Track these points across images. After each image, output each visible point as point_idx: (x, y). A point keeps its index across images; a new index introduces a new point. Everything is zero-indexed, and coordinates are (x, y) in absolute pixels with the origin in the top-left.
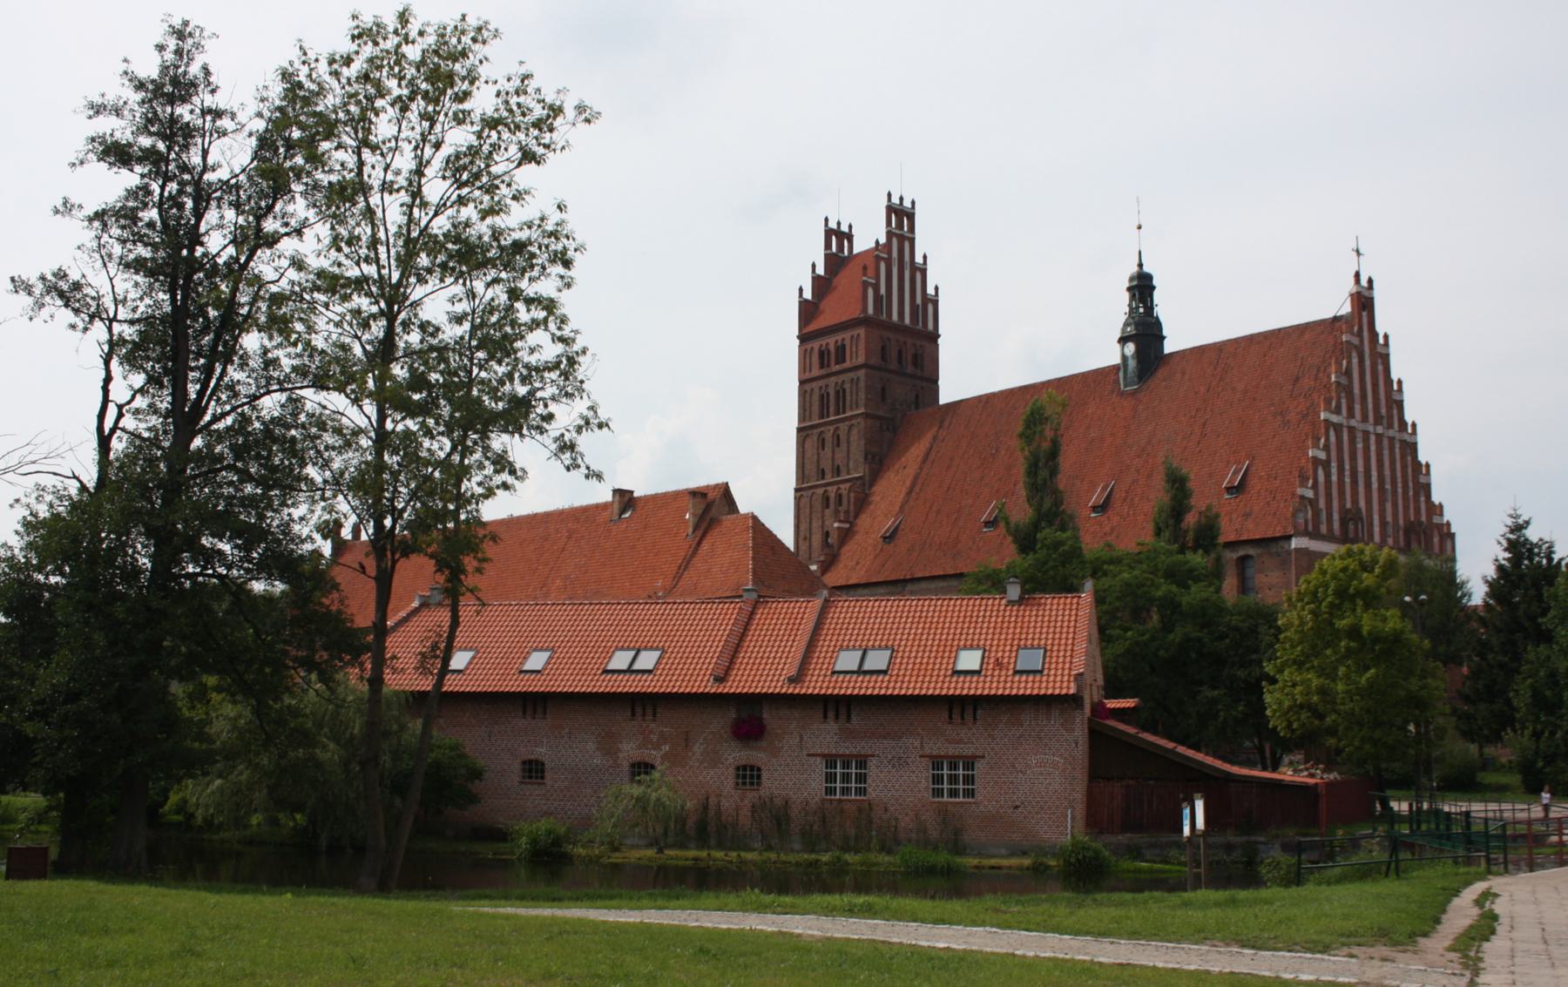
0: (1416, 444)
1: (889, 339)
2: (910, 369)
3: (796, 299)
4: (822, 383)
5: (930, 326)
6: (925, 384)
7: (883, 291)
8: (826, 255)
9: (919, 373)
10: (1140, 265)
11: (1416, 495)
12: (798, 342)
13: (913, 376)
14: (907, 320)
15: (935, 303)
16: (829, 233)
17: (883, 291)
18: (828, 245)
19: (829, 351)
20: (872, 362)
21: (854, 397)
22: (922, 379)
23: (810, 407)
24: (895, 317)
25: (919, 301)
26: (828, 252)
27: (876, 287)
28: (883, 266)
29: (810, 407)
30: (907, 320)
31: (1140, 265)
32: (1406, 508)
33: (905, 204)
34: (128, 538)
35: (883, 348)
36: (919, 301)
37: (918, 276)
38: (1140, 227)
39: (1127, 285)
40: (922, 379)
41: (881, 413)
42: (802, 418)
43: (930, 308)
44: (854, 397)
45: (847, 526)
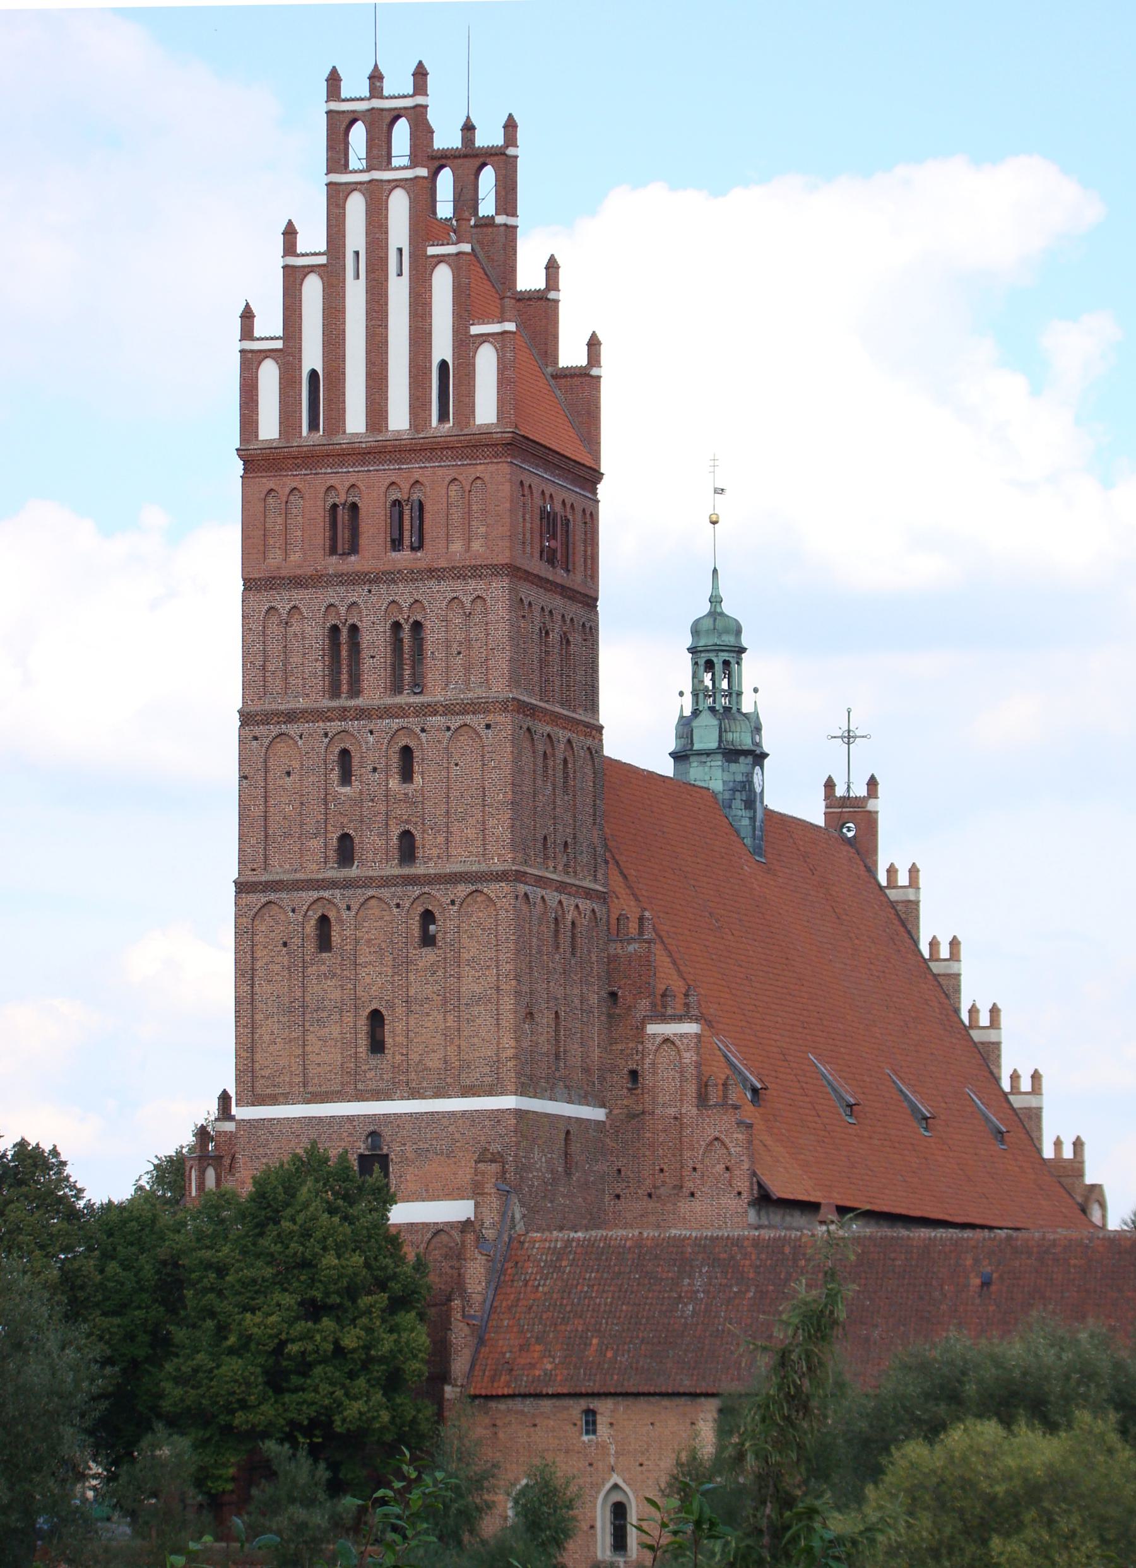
4: (331, 595)
7: (312, 358)
10: (716, 600)
14: (399, 419)
17: (312, 358)
24: (355, 421)
28: (312, 289)
30: (399, 419)
31: (716, 600)
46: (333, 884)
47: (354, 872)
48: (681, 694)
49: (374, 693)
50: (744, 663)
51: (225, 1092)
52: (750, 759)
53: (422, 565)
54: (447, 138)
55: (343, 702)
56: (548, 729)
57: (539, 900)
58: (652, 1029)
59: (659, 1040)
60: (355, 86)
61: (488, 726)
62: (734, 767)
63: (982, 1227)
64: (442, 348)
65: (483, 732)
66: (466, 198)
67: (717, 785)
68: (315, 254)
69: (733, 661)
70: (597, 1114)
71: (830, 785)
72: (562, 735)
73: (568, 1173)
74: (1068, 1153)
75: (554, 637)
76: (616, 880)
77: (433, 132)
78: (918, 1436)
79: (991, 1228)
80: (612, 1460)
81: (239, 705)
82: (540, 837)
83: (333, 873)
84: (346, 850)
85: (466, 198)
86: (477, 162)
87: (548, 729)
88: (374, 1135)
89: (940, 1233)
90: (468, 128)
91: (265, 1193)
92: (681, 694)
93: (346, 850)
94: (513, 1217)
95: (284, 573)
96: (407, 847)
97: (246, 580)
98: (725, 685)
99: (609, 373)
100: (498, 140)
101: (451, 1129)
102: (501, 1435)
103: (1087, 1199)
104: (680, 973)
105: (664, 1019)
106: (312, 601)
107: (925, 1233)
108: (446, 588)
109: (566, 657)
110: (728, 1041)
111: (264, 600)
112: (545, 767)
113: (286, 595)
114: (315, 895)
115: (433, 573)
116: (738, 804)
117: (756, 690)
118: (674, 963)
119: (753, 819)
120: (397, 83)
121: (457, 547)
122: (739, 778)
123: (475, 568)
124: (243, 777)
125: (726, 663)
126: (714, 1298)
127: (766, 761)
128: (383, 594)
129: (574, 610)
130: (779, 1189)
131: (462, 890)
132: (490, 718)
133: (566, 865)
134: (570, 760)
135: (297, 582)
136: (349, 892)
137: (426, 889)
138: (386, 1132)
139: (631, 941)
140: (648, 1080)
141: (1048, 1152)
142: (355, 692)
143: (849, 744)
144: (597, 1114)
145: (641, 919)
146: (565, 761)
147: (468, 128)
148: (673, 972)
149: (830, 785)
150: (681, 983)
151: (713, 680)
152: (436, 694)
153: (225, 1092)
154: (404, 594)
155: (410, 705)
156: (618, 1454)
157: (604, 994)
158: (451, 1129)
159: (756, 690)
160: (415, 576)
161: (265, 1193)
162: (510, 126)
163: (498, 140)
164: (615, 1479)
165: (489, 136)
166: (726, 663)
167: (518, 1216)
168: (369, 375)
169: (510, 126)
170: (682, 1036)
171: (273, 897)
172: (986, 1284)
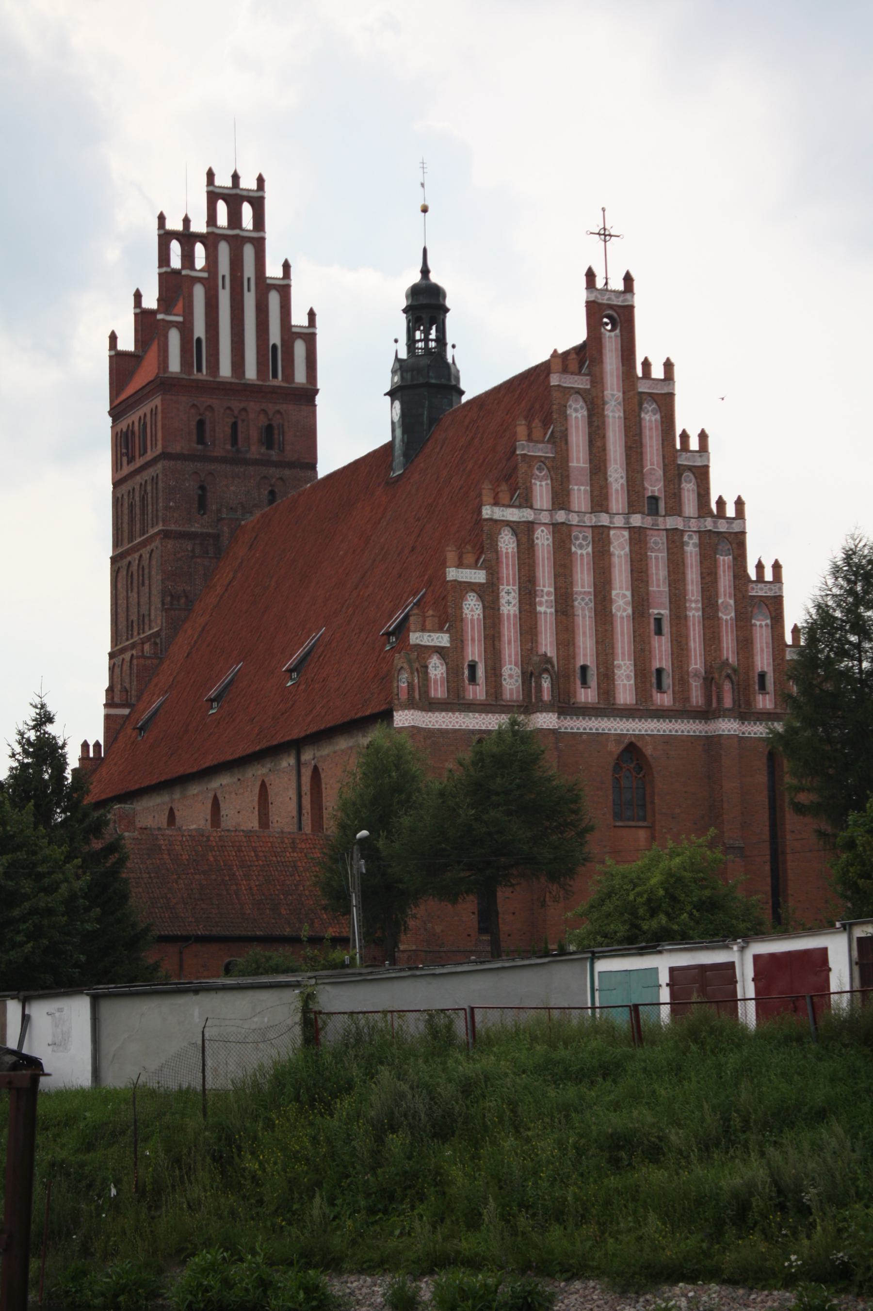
0: (743, 533)
1: (210, 408)
2: (255, 451)
3: (105, 354)
5: (300, 376)
6: (287, 472)
7: (199, 330)
8: (160, 275)
9: (274, 455)
10: (425, 272)
11: (743, 621)
12: (109, 420)
13: (266, 463)
14: (251, 372)
15: (310, 339)
16: (165, 237)
17: (199, 330)
18: (164, 258)
19: (133, 433)
20: (177, 448)
21: (155, 507)
22: (291, 465)
23: (122, 516)
24: (225, 370)
25: (275, 337)
26: (164, 270)
27: (186, 329)
29: (122, 516)
30: (251, 372)
31: (425, 272)
32: (712, 638)
33: (243, 184)
34: (60, 813)
35: (201, 424)
36: (275, 337)
37: (274, 299)
38: (425, 210)
39: (404, 303)
40: (291, 465)
41: (196, 528)
42: (117, 543)
43: (300, 348)
44: (155, 507)
45: (126, 711)
48: (396, 341)
70: (103, 756)
71: (590, 275)
78: (104, 1088)
90: (236, 177)
92: (396, 341)
143: (599, 234)
144: (103, 756)
147: (236, 177)
149: (590, 275)
162: (261, 180)
168: (233, 342)
169: (261, 180)
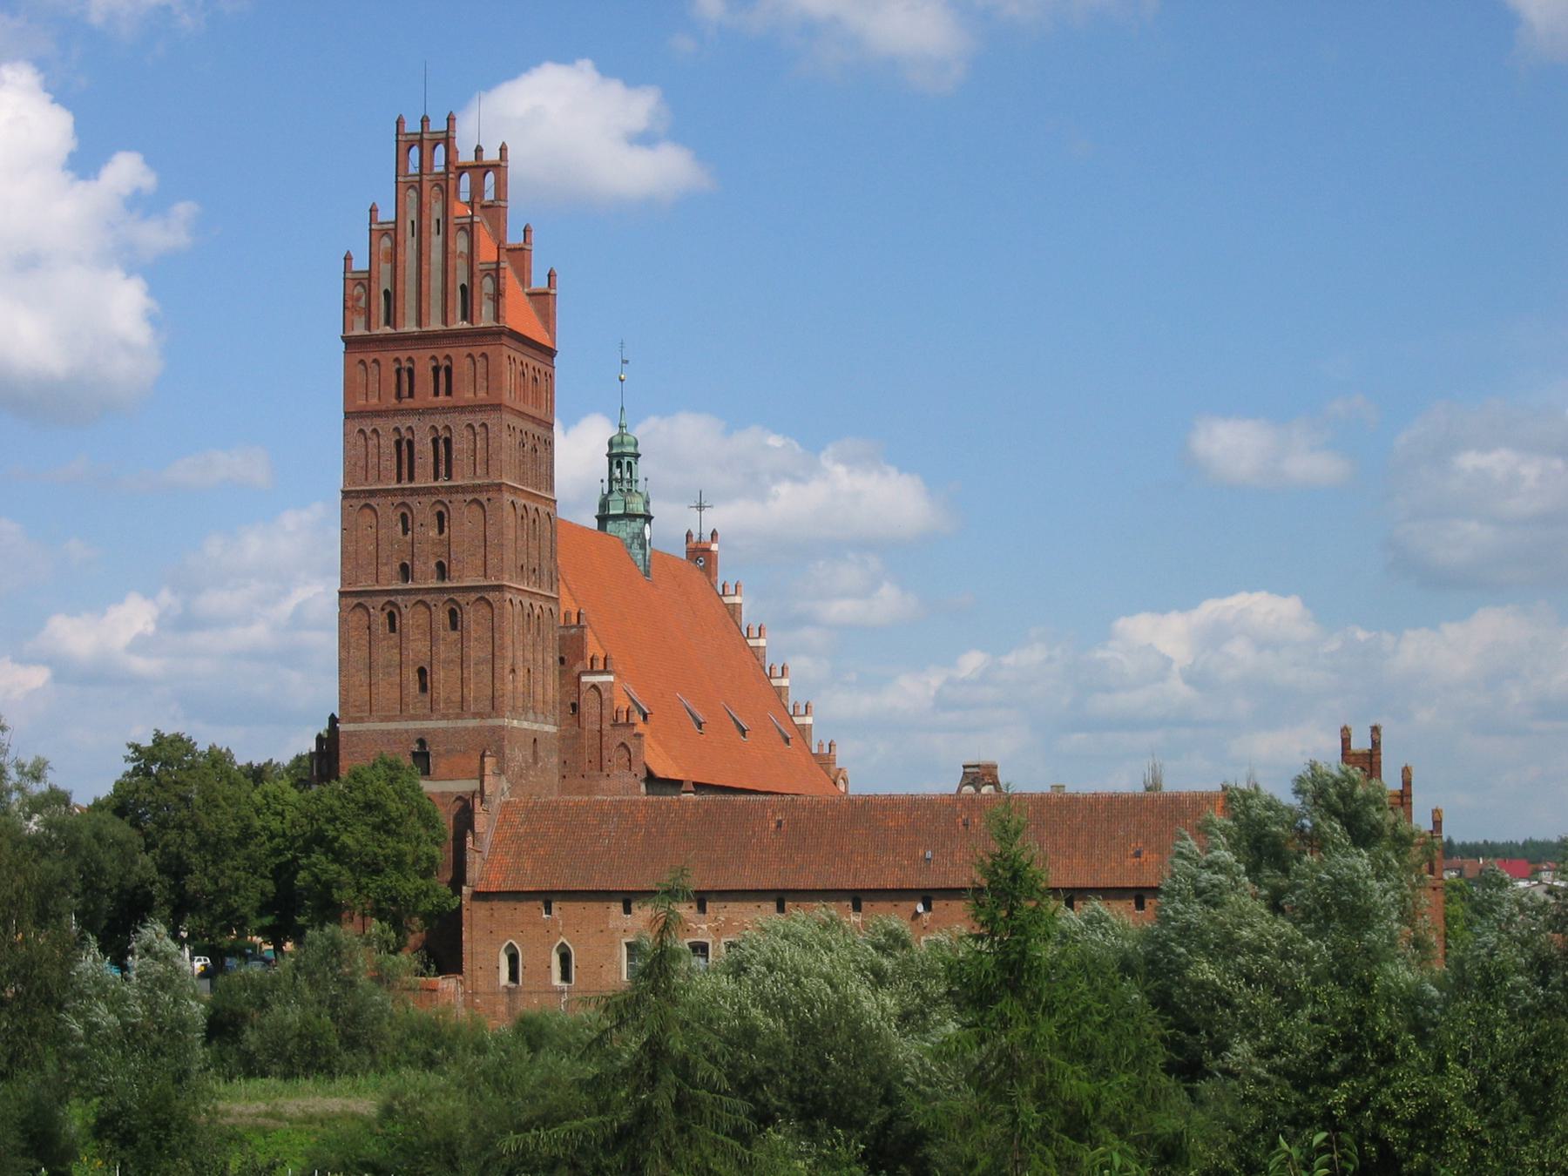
4: (399, 422)
46: (397, 592)
47: (410, 585)
48: (602, 481)
49: (424, 480)
50: (639, 463)
51: (333, 715)
52: (643, 520)
53: (451, 404)
54: (466, 156)
55: (406, 485)
56: (523, 502)
57: (518, 603)
58: (584, 679)
59: (589, 686)
60: (412, 126)
61: (489, 500)
62: (633, 524)
63: (777, 793)
64: (462, 278)
65: (485, 504)
66: (477, 190)
67: (623, 535)
68: (388, 223)
69: (633, 462)
72: (532, 505)
73: (535, 762)
74: (826, 750)
75: (528, 447)
76: (563, 589)
77: (458, 152)
79: (782, 794)
80: (561, 929)
81: (341, 486)
82: (519, 566)
83: (401, 586)
84: (405, 572)
85: (477, 190)
86: (484, 170)
87: (523, 502)
88: (422, 742)
89: (753, 797)
90: (479, 150)
91: (611, 725)
93: (405, 572)
94: (503, 789)
95: (369, 409)
96: (442, 571)
97: (345, 413)
98: (628, 476)
99: (560, 290)
100: (496, 157)
101: (466, 737)
102: (496, 915)
103: (837, 777)
104: (602, 647)
105: (592, 672)
106: (386, 426)
107: (742, 798)
108: (467, 418)
109: (535, 460)
110: (630, 686)
111: (357, 425)
112: (523, 523)
113: (369, 422)
114: (386, 599)
115: (462, 409)
116: (635, 546)
117: (646, 479)
118: (598, 639)
119: (645, 555)
120: (438, 125)
121: (470, 395)
122: (636, 531)
123: (481, 406)
124: (344, 529)
125: (629, 464)
126: (1536, 1054)
127: (653, 521)
128: (429, 421)
129: (539, 431)
130: (660, 772)
131: (473, 596)
132: (490, 495)
133: (535, 582)
134: (537, 520)
135: (378, 414)
136: (407, 597)
137: (452, 596)
138: (428, 738)
139: (572, 627)
140: (584, 708)
141: (815, 751)
142: (411, 478)
145: (579, 614)
146: (534, 521)
147: (479, 150)
148: (597, 645)
150: (602, 651)
151: (621, 472)
152: (458, 481)
153: (333, 715)
154: (440, 421)
155: (442, 487)
156: (564, 926)
157: (557, 658)
158: (466, 737)
159: (646, 479)
160: (445, 410)
161: (611, 725)
163: (496, 157)
164: (563, 939)
165: (491, 155)
166: (629, 464)
167: (506, 789)
169: (503, 149)
170: (602, 683)
171: (361, 600)
172: (779, 824)
